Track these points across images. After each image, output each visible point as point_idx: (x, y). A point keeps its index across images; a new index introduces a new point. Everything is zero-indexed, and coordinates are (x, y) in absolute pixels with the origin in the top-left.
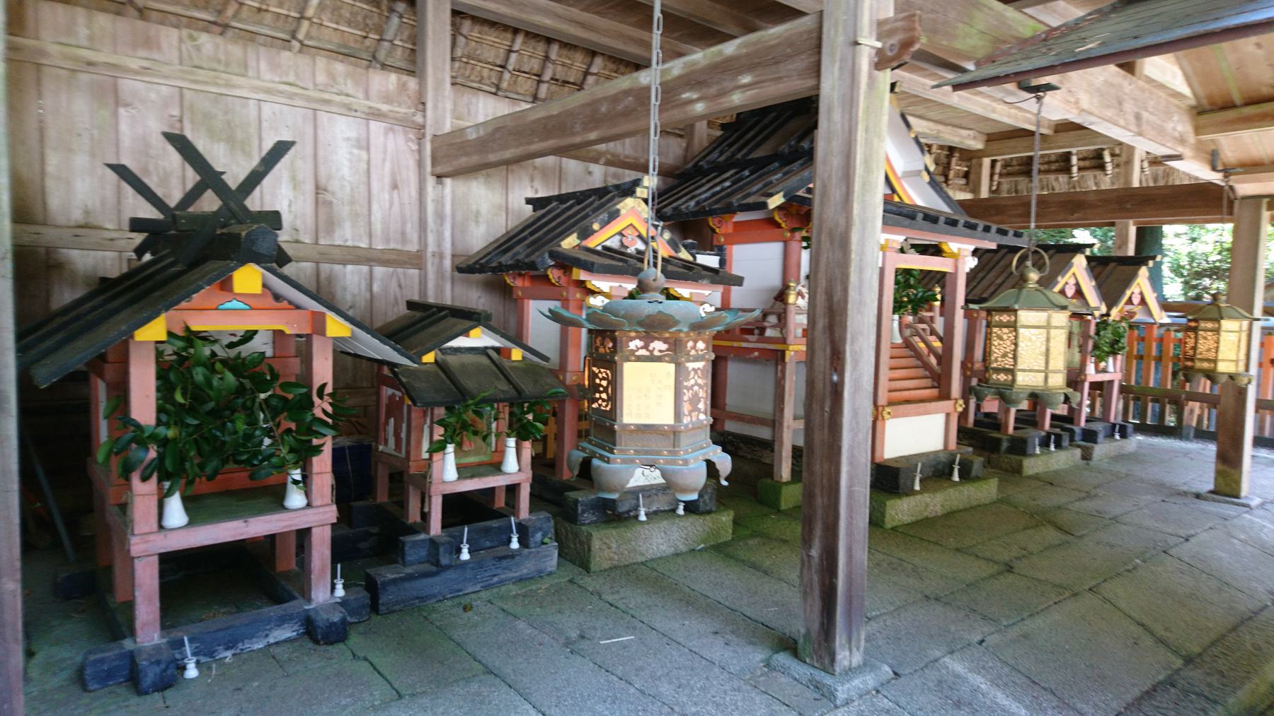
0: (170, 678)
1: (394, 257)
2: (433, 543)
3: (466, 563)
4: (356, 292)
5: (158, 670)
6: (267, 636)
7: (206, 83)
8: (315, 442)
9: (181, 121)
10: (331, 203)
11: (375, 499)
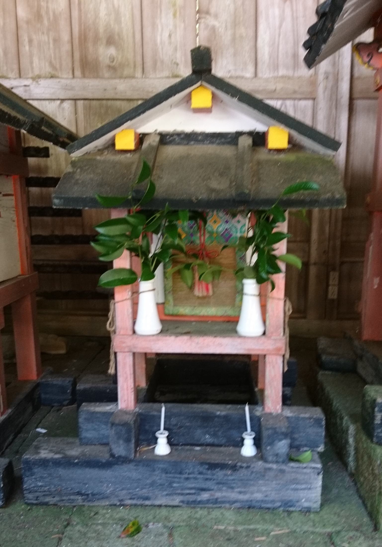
3: (162, 459)
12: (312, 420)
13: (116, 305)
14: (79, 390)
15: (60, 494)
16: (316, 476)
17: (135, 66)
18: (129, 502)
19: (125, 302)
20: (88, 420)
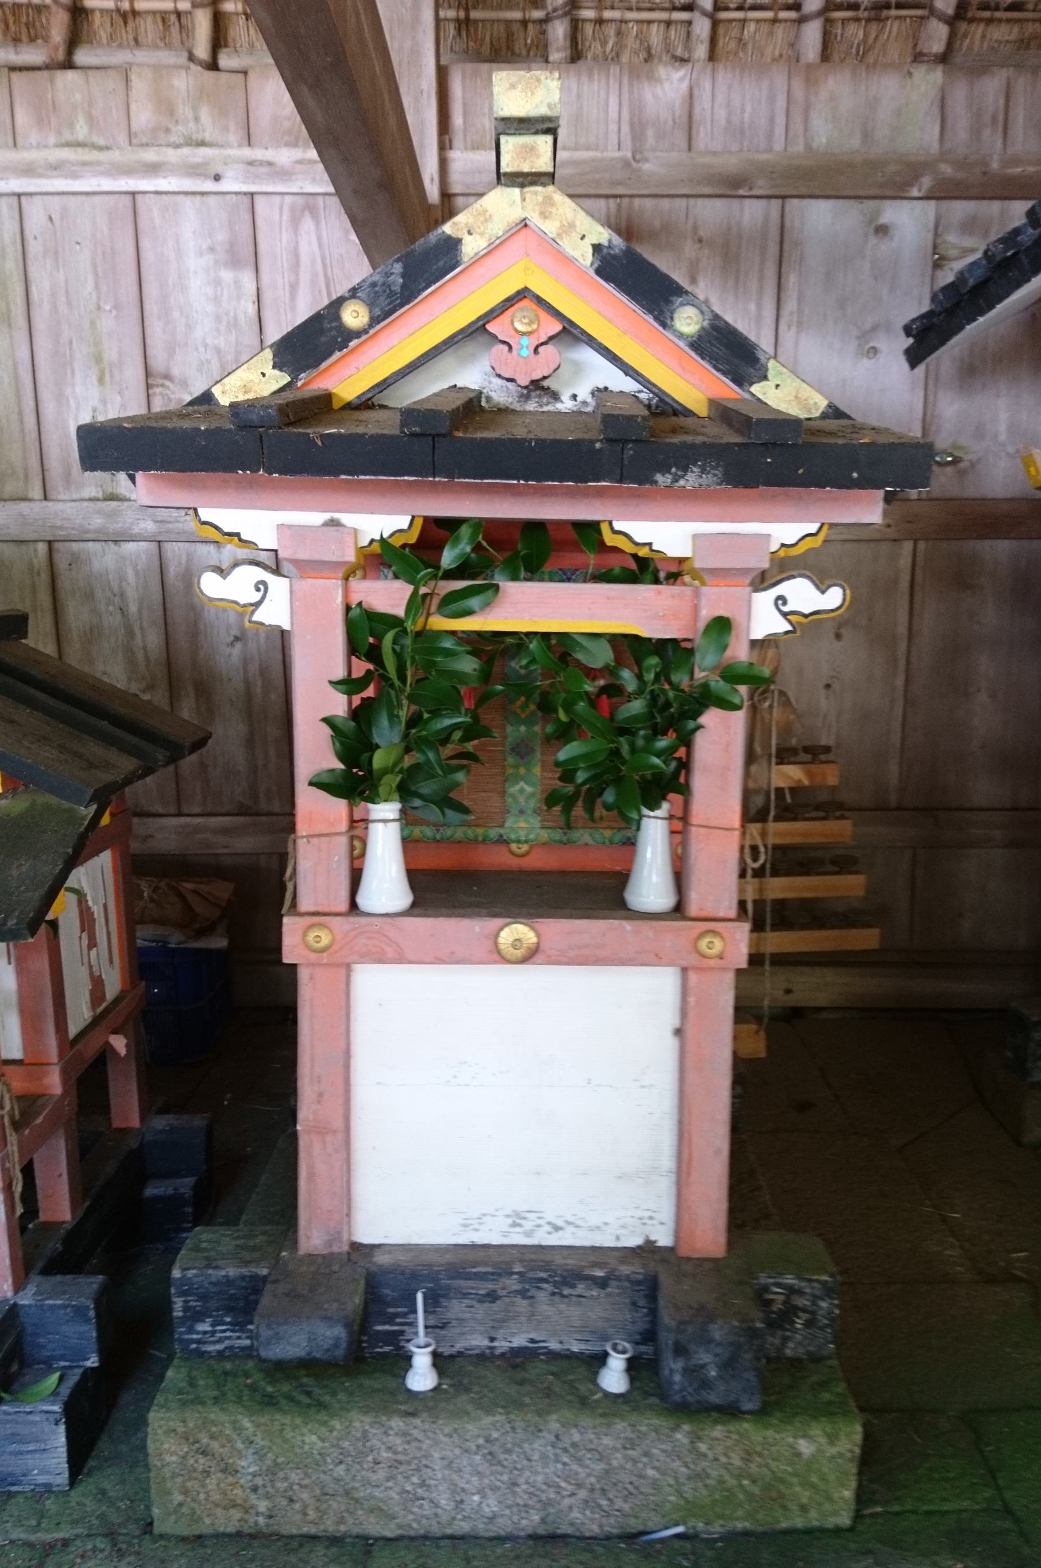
12: (69, 1309)
16: (54, 1427)
17: (26, 477)
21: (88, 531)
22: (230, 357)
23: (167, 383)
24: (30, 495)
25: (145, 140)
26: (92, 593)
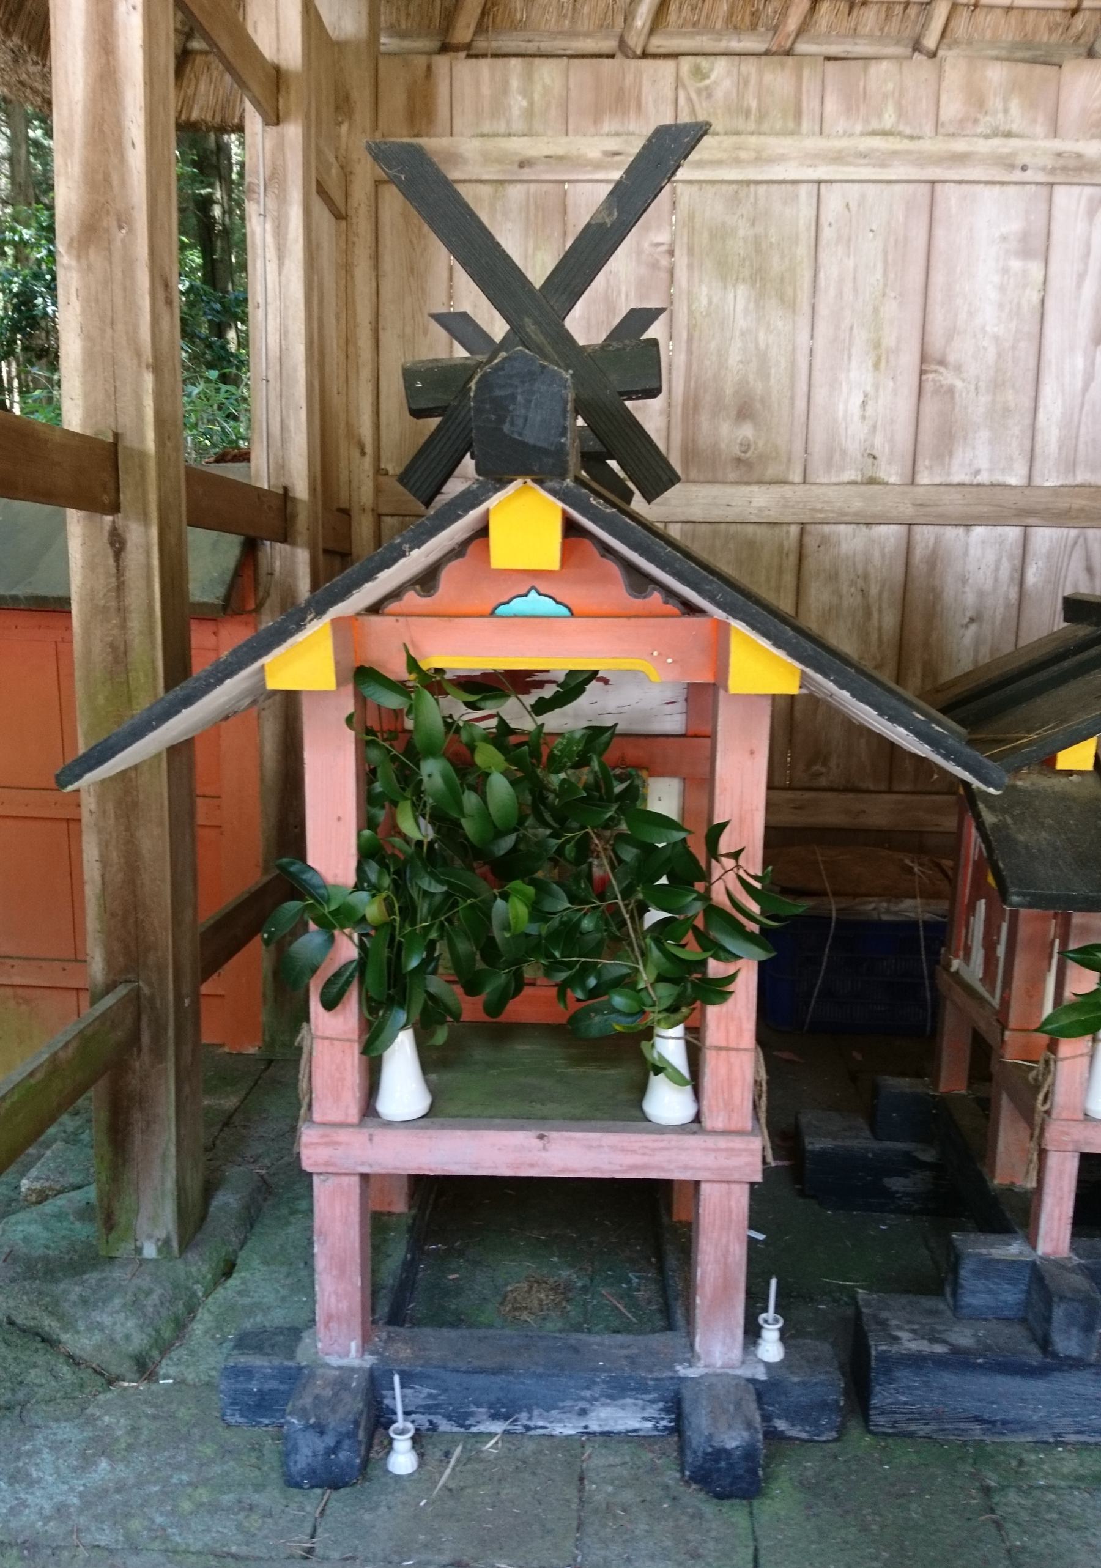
0: (349, 1467)
1: (1078, 503)
2: (1037, 1277)
4: (989, 585)
5: (321, 1444)
6: (583, 1412)
7: (719, 163)
8: (715, 968)
9: (671, 253)
10: (951, 391)
11: (935, 1083)
13: (1060, 1064)
14: (812, 1152)
15: (939, 1418)
17: (789, 460)
18: (1073, 1438)
19: (1078, 1060)
20: (976, 1273)
21: (846, 514)
22: (1007, 345)
23: (941, 369)
24: (791, 478)
25: (952, 130)
26: (837, 574)
